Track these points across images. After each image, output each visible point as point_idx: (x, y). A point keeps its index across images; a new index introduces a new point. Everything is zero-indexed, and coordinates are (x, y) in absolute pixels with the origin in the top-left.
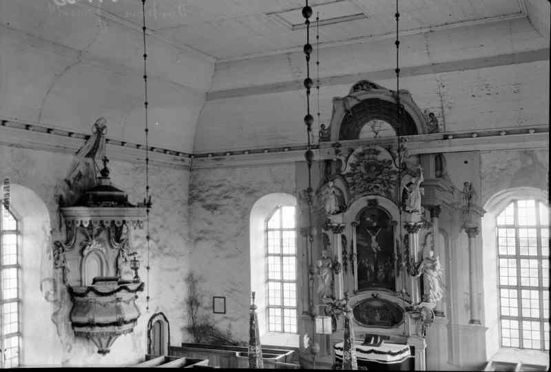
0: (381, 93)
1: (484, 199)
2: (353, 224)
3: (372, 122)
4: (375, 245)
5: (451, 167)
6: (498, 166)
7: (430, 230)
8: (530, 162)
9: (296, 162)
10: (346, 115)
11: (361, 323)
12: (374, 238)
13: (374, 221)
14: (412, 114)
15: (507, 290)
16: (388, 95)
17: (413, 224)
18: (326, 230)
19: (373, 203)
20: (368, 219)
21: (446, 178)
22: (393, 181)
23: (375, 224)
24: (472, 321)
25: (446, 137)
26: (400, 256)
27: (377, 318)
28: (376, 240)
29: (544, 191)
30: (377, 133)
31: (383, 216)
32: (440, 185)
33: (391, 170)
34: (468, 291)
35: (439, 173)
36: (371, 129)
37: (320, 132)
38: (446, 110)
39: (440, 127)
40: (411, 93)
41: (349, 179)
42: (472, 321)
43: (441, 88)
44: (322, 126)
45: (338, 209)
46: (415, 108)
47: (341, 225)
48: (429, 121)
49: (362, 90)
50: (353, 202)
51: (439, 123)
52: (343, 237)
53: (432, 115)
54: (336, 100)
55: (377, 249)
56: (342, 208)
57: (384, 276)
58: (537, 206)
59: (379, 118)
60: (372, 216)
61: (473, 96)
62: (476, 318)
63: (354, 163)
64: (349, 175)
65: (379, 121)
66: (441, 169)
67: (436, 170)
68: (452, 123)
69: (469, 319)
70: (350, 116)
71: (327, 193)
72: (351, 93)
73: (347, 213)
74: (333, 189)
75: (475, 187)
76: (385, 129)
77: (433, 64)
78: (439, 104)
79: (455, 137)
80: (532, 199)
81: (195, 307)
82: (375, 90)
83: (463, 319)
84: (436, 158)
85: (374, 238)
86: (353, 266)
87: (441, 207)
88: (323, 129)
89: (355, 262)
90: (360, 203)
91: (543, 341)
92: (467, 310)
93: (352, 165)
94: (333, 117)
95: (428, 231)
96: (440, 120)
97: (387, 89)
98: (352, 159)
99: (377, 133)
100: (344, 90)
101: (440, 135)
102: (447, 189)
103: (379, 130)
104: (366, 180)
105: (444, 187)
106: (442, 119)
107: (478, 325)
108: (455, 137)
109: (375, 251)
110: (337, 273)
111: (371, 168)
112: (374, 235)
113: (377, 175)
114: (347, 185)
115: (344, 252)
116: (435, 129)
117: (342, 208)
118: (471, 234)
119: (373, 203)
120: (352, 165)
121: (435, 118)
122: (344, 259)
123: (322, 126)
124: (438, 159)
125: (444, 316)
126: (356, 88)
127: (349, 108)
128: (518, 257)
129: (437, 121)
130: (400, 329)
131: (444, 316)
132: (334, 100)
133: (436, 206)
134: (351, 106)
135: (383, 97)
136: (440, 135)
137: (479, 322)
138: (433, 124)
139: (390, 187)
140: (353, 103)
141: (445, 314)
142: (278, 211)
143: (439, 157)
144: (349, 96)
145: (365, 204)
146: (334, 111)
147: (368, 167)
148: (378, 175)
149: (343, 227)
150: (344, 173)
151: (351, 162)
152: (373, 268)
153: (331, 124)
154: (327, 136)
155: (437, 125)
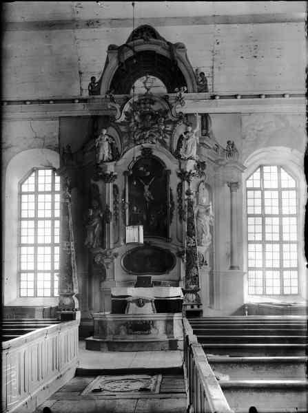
0: (158, 44)
1: (244, 157)
2: (125, 173)
3: (145, 78)
4: (147, 193)
5: (215, 125)
6: (256, 128)
7: (203, 178)
8: (283, 125)
9: (60, 117)
10: (119, 68)
11: (131, 272)
12: (146, 187)
13: (147, 171)
14: (185, 72)
15: (274, 240)
16: (164, 48)
17: (188, 171)
18: (96, 180)
19: (147, 152)
20: (142, 169)
21: (211, 137)
22: (168, 131)
23: (148, 173)
24: (232, 268)
25: (213, 97)
26: (173, 204)
27: (148, 265)
28: (149, 189)
29: (295, 151)
30: (148, 90)
31: (158, 165)
32: (206, 143)
33: (167, 120)
34: (229, 240)
35: (204, 131)
36: (143, 85)
37: (90, 84)
38: (216, 70)
39: (209, 87)
40: (187, 48)
41: (123, 129)
42: (232, 268)
43: (216, 45)
44: (93, 78)
45: (111, 157)
46: (186, 62)
47: (114, 174)
48: (199, 80)
49: (142, 38)
50: (127, 150)
51: (208, 83)
52: (115, 186)
53: (202, 74)
54: (112, 48)
55: (149, 198)
56: (116, 156)
57: (156, 225)
58: (279, 172)
59: (151, 74)
60: (145, 166)
61: (242, 57)
62: (234, 265)
63: (129, 112)
64: (122, 123)
65: (152, 77)
66: (207, 129)
67: (202, 129)
68: (219, 84)
69: (229, 266)
70: (123, 70)
71: (101, 139)
72: (127, 42)
73: (120, 162)
74: (107, 137)
75: (237, 145)
76: (157, 86)
77: (214, 16)
78: (210, 63)
79: (221, 97)
80: (241, 175)
81: (97, 79)
82: (155, 40)
83: (223, 267)
84: (202, 119)
85: (146, 187)
86: (124, 213)
87: (206, 163)
88: (94, 83)
89: (127, 211)
90: (134, 152)
91: (52, 289)
92: (228, 258)
93: (126, 113)
94: (105, 69)
95: (202, 179)
96: (209, 80)
97: (164, 40)
98: (127, 108)
99: (148, 90)
100: (122, 36)
101: (207, 95)
102: (212, 147)
103: (148, 85)
104: (140, 129)
105: (209, 145)
106: (211, 79)
107: (238, 271)
108: (221, 97)
109: (147, 199)
110: (109, 223)
111: (147, 117)
112: (147, 184)
113: (152, 124)
114: (121, 134)
115: (115, 202)
116: (203, 88)
117: (116, 156)
118: (233, 188)
119: (147, 152)
120: (126, 113)
121: (205, 78)
122: (115, 209)
123: (93, 78)
124: (204, 119)
125: (206, 265)
126: (136, 34)
127: (122, 61)
128: (263, 216)
129: (206, 81)
130: (172, 274)
131: (206, 265)
132: (109, 49)
133: (202, 163)
134: (125, 58)
135: (160, 50)
136: (207, 95)
137: (238, 268)
138: (202, 85)
139: (165, 137)
140: (130, 54)
141: (208, 263)
142: (34, 174)
143: (205, 117)
144: (124, 45)
145: (139, 153)
146: (107, 63)
147: (143, 116)
148: (154, 124)
149: (115, 176)
150: (118, 121)
151: (126, 110)
152: (145, 217)
153: (102, 78)
154: (96, 89)
155: (206, 85)
